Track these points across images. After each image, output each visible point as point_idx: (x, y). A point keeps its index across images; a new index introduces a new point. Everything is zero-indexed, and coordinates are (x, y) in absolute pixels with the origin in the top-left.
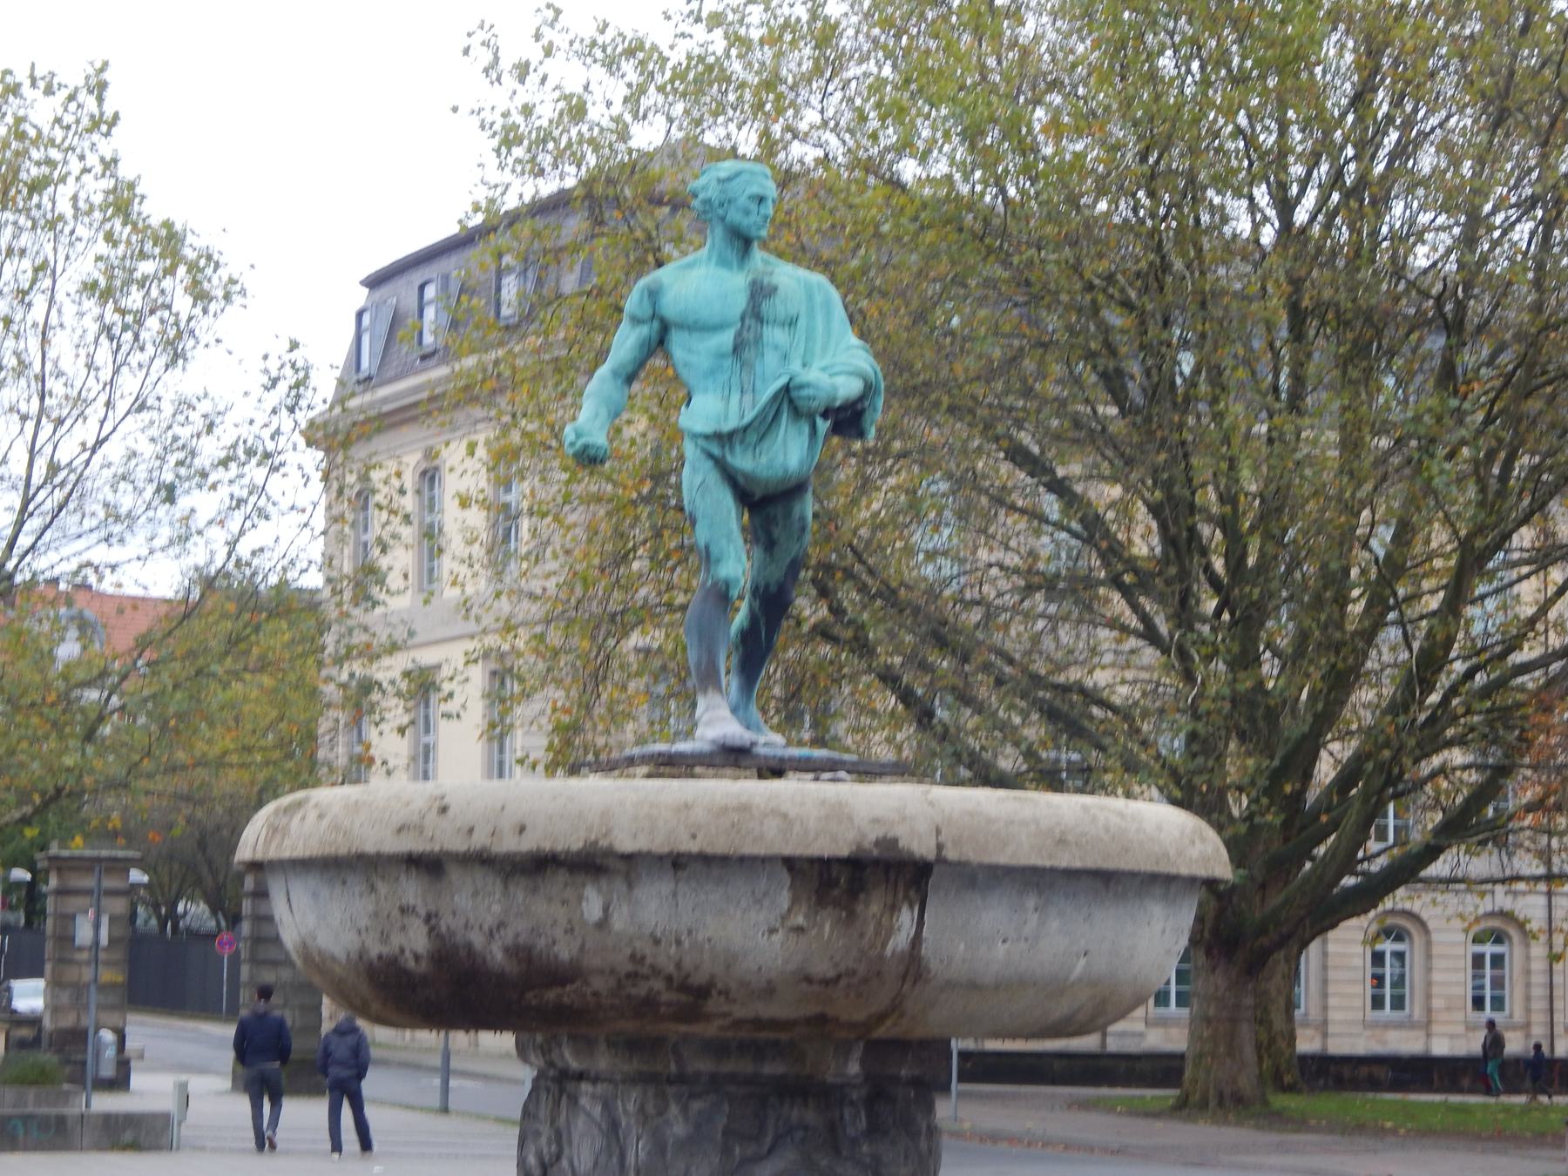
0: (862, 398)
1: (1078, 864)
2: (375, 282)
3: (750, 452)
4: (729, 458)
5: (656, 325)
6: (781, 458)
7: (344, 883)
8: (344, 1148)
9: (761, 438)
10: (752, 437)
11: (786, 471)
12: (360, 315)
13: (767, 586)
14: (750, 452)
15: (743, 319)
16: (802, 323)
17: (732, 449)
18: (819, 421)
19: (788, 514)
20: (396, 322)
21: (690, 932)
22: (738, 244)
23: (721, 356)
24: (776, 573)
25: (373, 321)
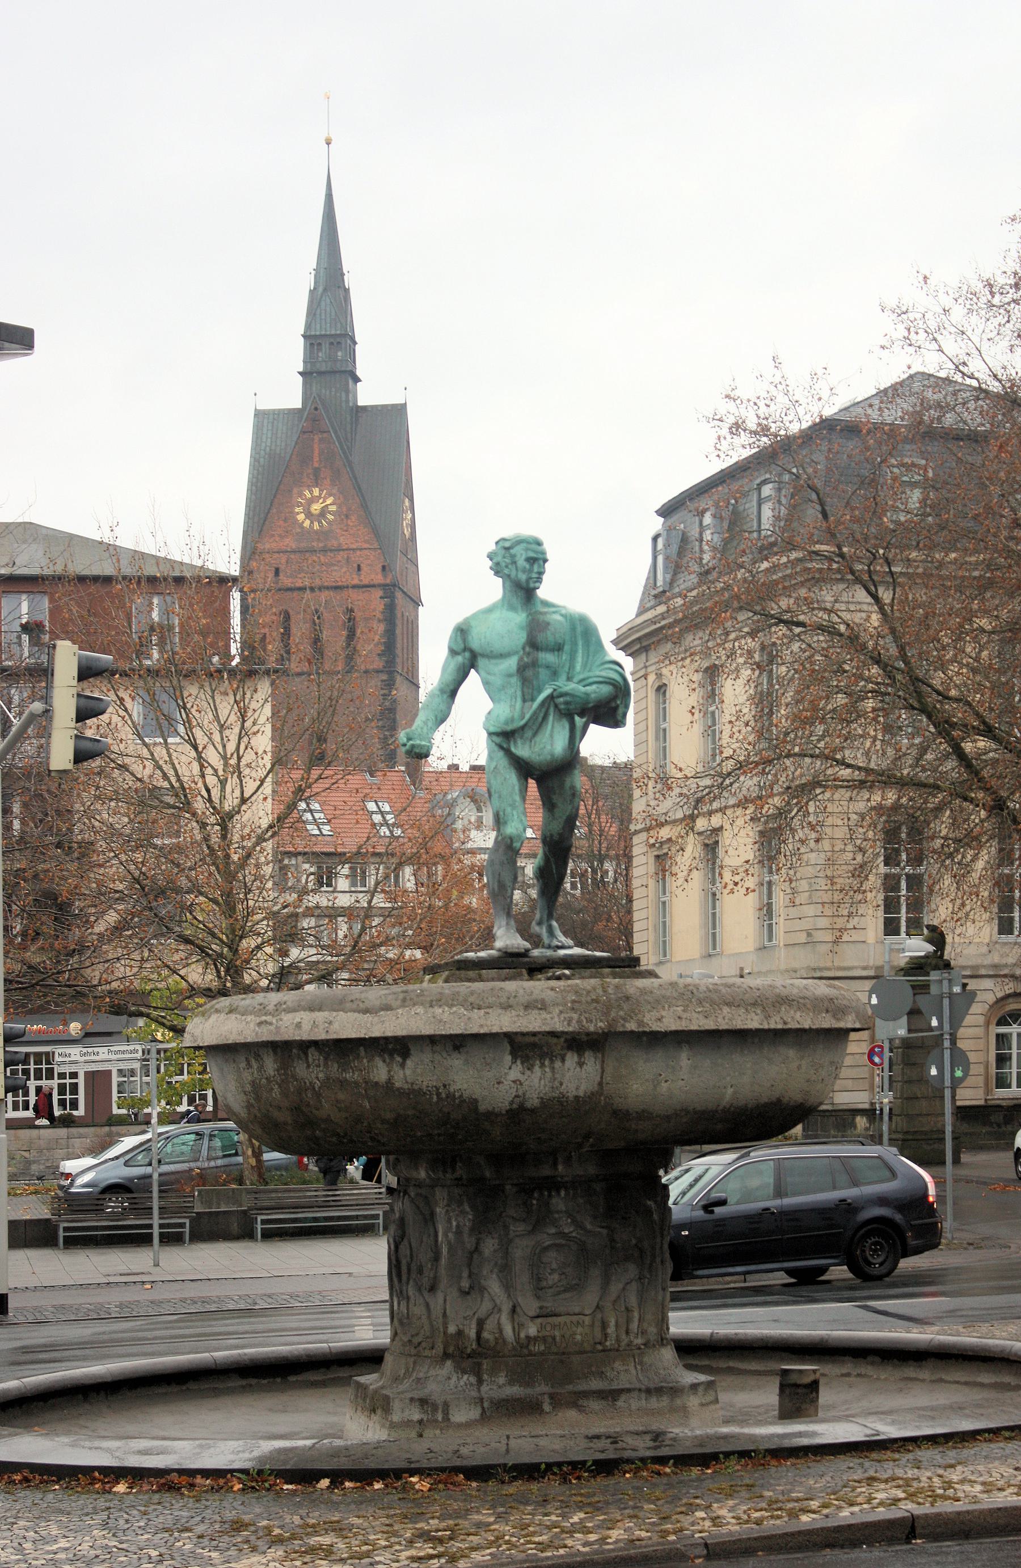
0: (614, 698)
1: (724, 1026)
2: (667, 511)
3: (528, 743)
4: (513, 749)
5: (467, 654)
6: (549, 747)
7: (234, 1061)
8: (21, 1255)
9: (535, 734)
10: (529, 734)
11: (552, 755)
12: (655, 539)
13: (552, 836)
14: (528, 743)
15: (524, 648)
16: (567, 648)
17: (515, 742)
18: (577, 718)
19: (562, 786)
20: (684, 539)
21: (445, 1086)
22: (521, 594)
23: (510, 676)
24: (557, 827)
25: (667, 545)
